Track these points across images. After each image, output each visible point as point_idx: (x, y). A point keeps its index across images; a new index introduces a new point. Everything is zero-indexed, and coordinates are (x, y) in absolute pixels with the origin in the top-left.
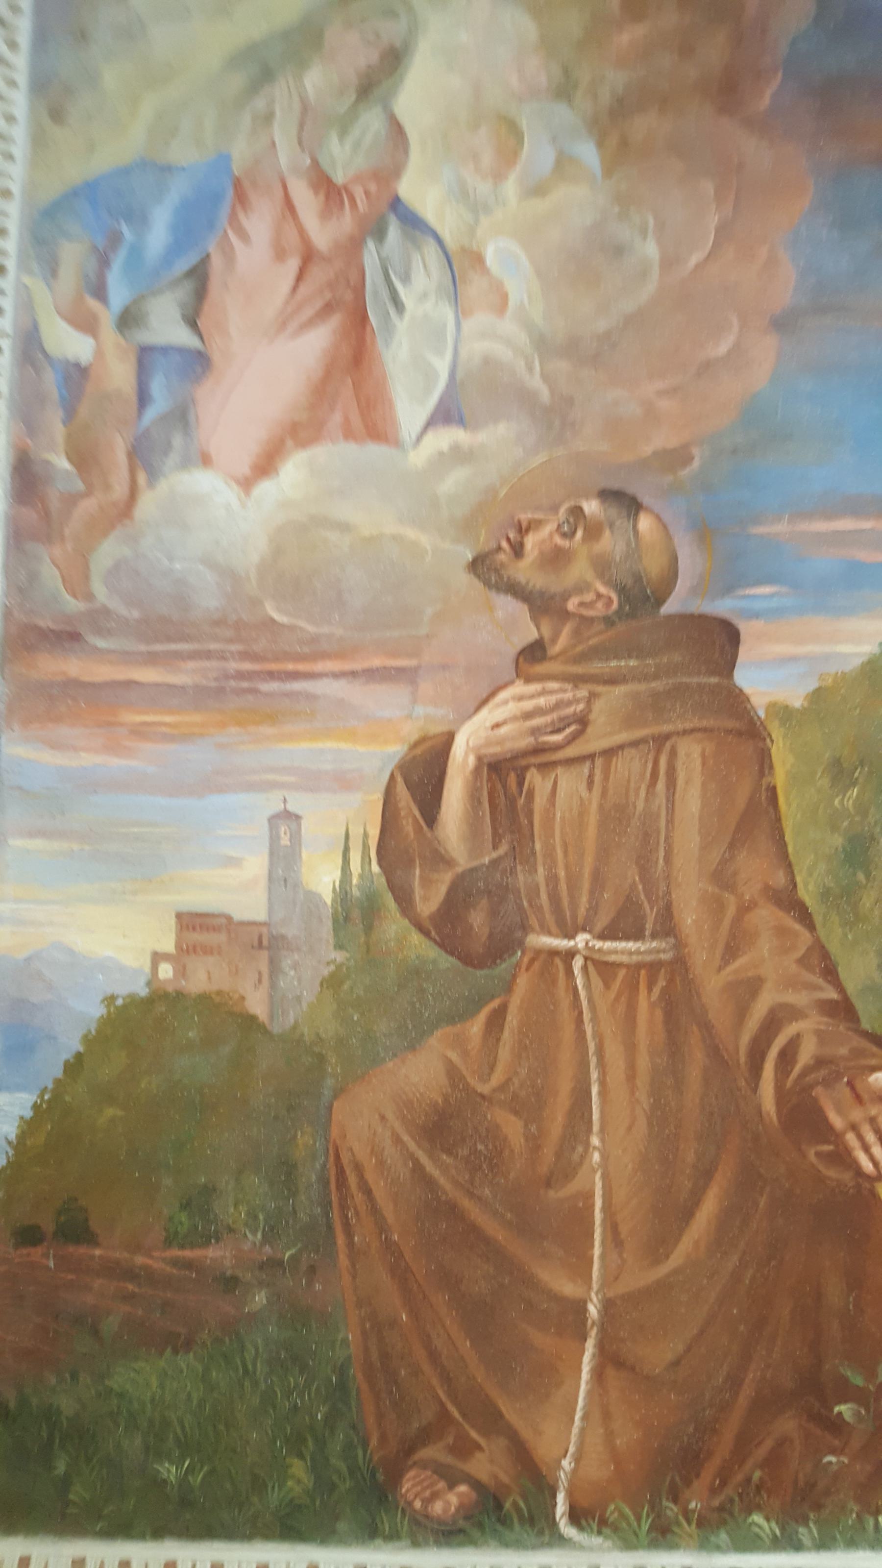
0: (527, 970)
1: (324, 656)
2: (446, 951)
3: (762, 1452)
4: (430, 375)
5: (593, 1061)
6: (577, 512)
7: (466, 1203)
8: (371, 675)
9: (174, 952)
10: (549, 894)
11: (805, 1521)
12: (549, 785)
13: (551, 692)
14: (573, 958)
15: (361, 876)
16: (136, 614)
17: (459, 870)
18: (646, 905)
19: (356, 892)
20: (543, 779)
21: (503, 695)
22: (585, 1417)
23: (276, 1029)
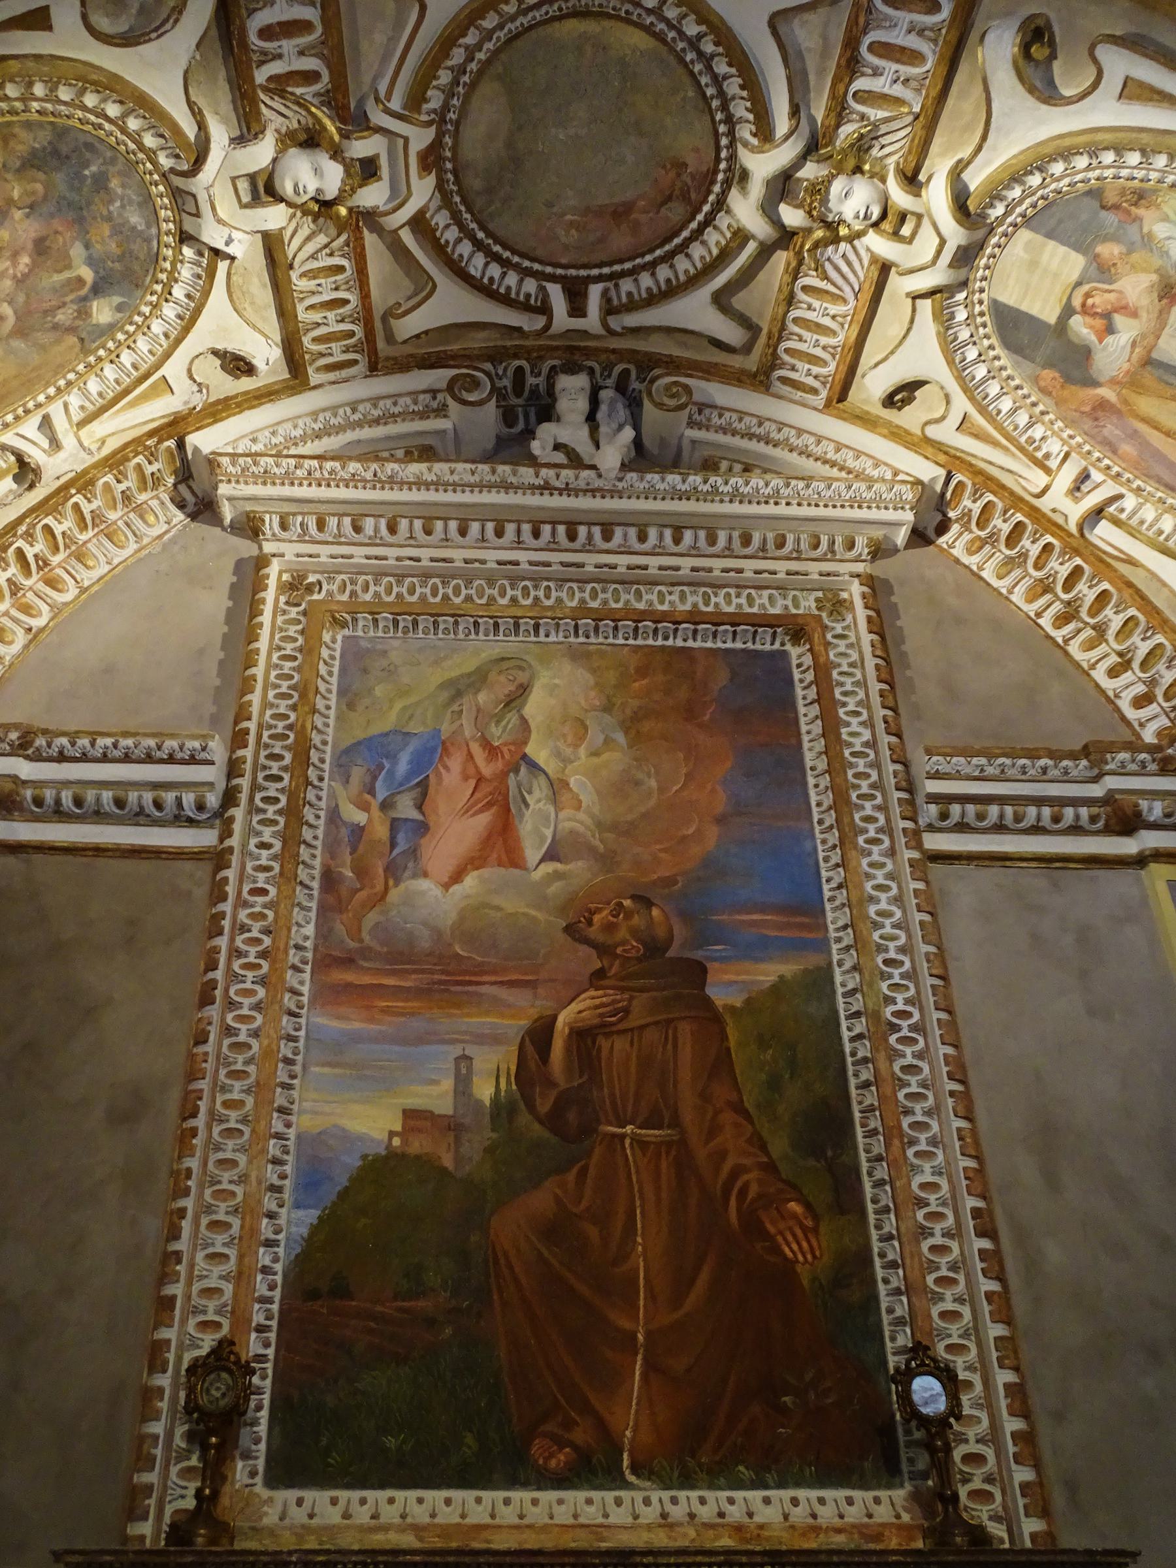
4: (542, 838)
6: (620, 905)
8: (511, 984)
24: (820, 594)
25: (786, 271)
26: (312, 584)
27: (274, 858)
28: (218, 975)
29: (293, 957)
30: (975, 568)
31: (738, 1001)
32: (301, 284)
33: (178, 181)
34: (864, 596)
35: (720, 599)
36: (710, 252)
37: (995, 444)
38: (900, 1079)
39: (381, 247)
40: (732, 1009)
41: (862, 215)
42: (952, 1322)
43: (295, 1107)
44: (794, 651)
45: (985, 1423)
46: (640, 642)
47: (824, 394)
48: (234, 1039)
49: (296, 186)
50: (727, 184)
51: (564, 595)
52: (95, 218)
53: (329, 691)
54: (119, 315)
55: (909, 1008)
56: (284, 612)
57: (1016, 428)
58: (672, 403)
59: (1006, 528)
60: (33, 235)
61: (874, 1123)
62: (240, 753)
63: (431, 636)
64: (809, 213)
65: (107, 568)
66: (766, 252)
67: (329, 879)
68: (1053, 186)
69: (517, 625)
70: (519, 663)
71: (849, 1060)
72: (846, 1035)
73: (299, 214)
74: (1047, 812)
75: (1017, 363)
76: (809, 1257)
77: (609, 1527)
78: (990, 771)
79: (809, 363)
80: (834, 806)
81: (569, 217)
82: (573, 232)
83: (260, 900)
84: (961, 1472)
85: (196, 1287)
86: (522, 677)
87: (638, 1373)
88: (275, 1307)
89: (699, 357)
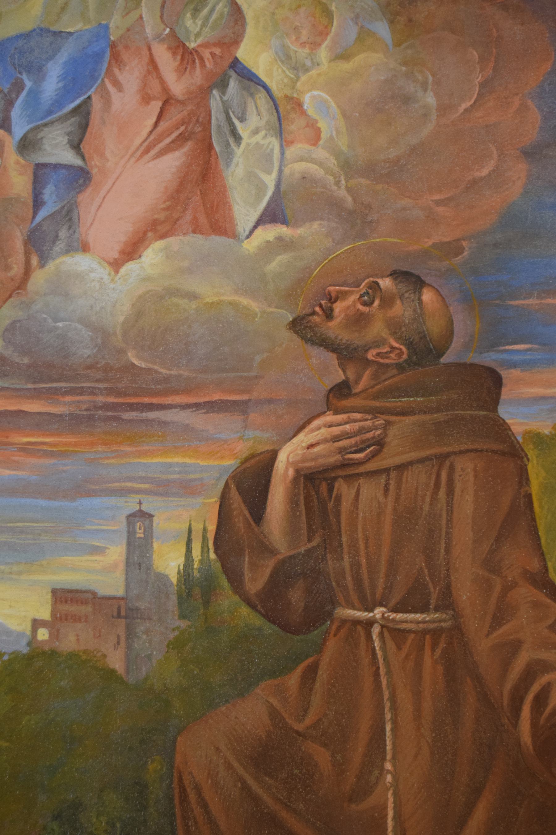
0: (335, 635)
2: (269, 621)
4: (261, 187)
6: (375, 286)
7: (284, 814)
9: (50, 619)
10: (353, 576)
12: (353, 492)
13: (355, 421)
14: (372, 627)
15: (201, 561)
16: (26, 361)
17: (280, 557)
18: (431, 585)
19: (196, 574)
20: (348, 487)
23: (131, 680)
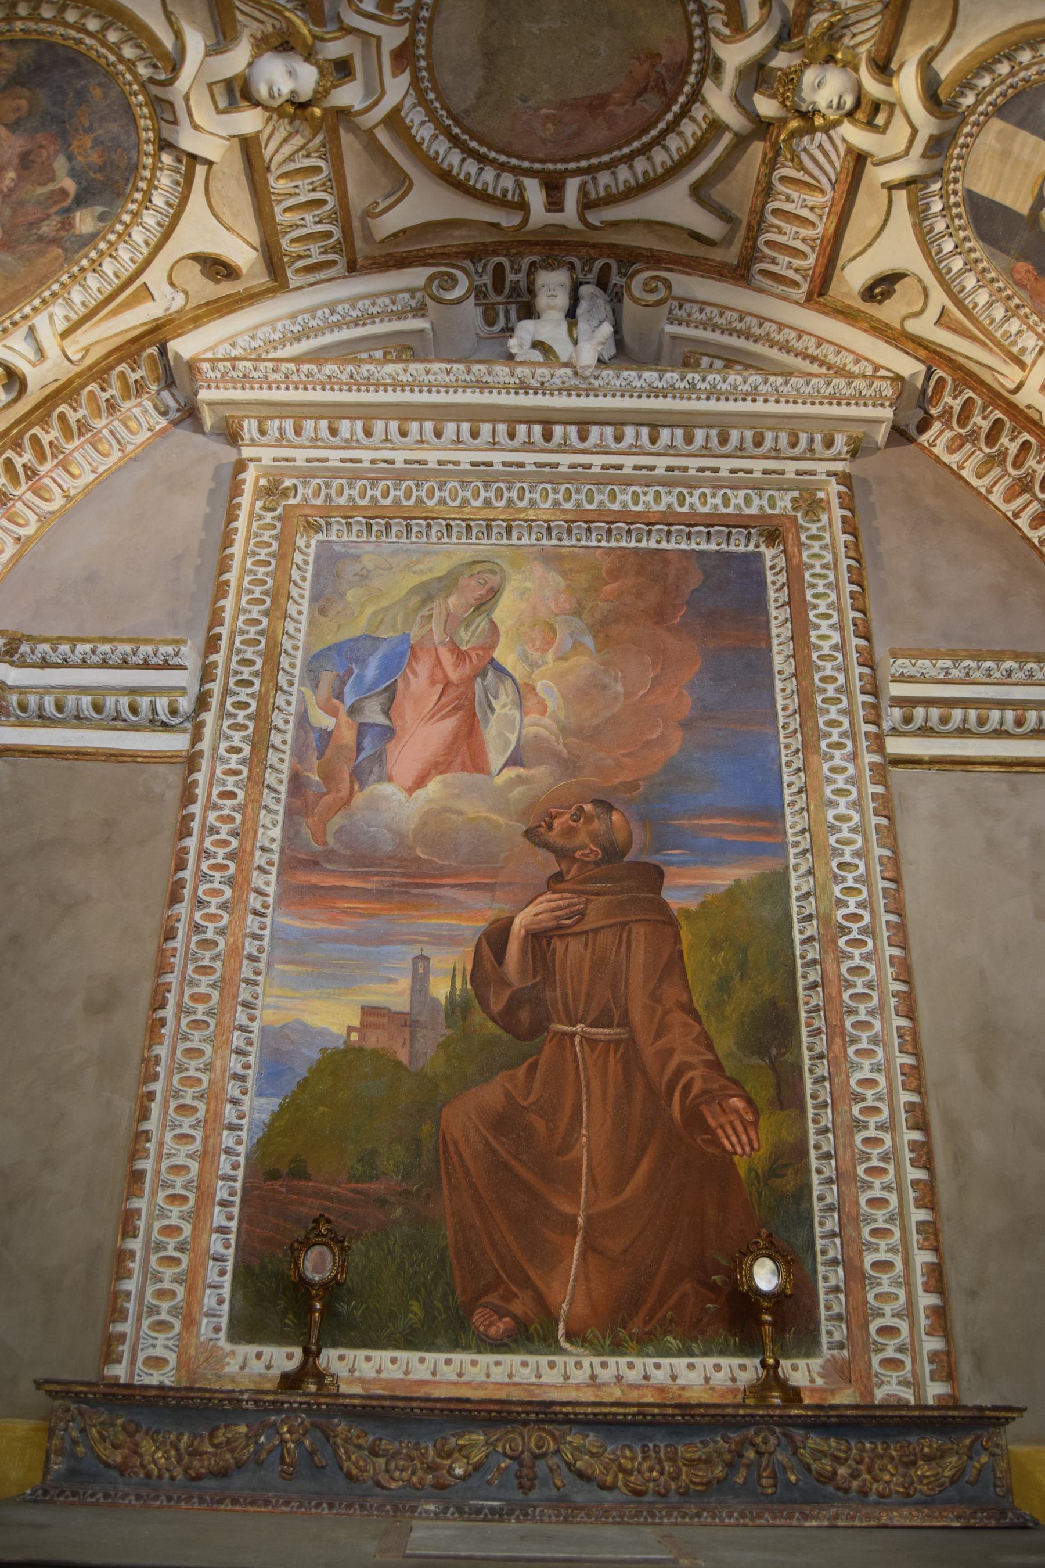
1: (448, 876)
3: (672, 1302)
4: (507, 742)
5: (584, 1090)
6: (581, 809)
7: (513, 1163)
8: (470, 886)
11: (695, 1340)
21: (540, 899)
22: (575, 1280)
23: (412, 1069)
24: (796, 494)
25: (763, 161)
26: (287, 488)
27: (243, 762)
28: (187, 874)
29: (260, 859)
30: (955, 467)
31: (693, 906)
32: (280, 186)
33: (155, 90)
34: (840, 495)
35: (695, 500)
36: (687, 144)
37: (974, 339)
38: (846, 980)
39: (358, 146)
40: (687, 913)
41: (835, 105)
42: (879, 1208)
43: (259, 1002)
44: (769, 553)
45: (902, 1299)
46: (613, 544)
47: (805, 287)
48: (202, 936)
49: (271, 89)
50: (702, 76)
51: (537, 496)
52: (77, 130)
53: (302, 597)
54: (101, 224)
55: (860, 911)
56: (260, 517)
57: (992, 321)
58: (652, 298)
59: (986, 425)
60: (18, 150)
61: (819, 1023)
62: (213, 658)
63: (404, 540)
64: (783, 103)
65: (93, 476)
66: (741, 142)
67: (297, 783)
68: (1022, 74)
69: (489, 527)
70: (490, 566)
71: (799, 962)
72: (797, 937)
73: (275, 117)
74: (1010, 715)
75: (992, 255)
76: (747, 1149)
77: (540, 1385)
78: (955, 673)
79: (790, 255)
80: (799, 711)
81: (544, 111)
82: (549, 125)
83: (229, 803)
84: (875, 1342)
85: (165, 1164)
86: (494, 580)
87: (576, 1253)
88: (238, 1185)
89: (679, 251)
